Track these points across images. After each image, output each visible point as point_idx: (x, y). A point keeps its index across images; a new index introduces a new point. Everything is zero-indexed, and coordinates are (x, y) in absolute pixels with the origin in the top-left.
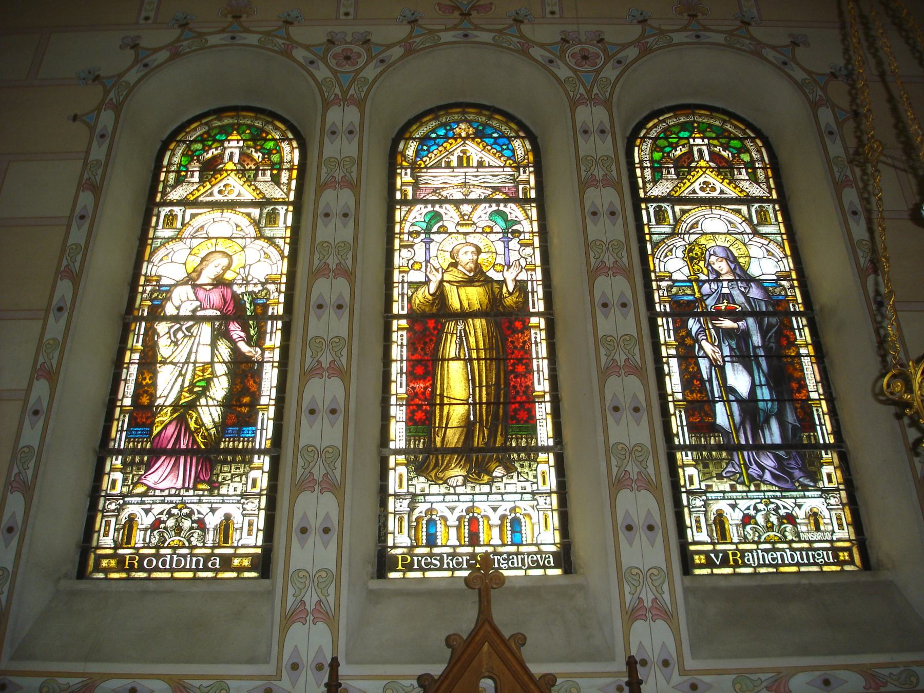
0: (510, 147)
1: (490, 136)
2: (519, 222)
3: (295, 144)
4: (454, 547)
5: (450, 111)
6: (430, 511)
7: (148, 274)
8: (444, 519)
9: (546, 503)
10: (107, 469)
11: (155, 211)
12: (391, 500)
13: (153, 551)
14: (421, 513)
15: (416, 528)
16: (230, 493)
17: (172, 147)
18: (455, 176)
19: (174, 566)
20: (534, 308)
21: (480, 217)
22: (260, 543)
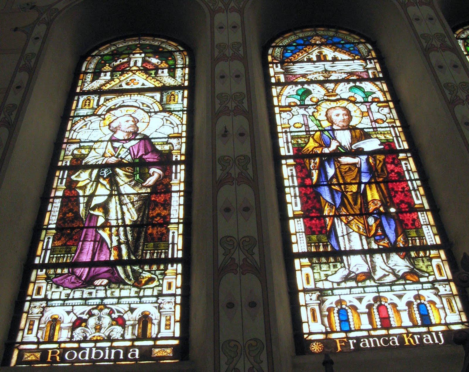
0: (356, 48)
1: (339, 43)
2: (374, 93)
3: (185, 53)
4: (368, 330)
5: (304, 30)
6: (340, 302)
7: (70, 137)
8: (354, 308)
9: (446, 290)
10: (33, 278)
11: (76, 98)
12: (301, 295)
13: (76, 345)
14: (332, 303)
15: (329, 317)
16: (131, 295)
17: (88, 59)
18: (301, 68)
19: (93, 357)
20: (400, 147)
21: (342, 90)
22: (177, 334)
